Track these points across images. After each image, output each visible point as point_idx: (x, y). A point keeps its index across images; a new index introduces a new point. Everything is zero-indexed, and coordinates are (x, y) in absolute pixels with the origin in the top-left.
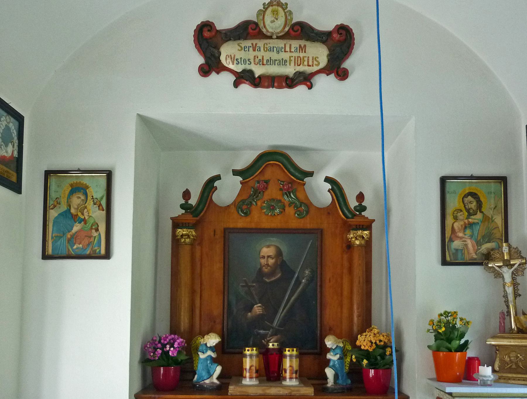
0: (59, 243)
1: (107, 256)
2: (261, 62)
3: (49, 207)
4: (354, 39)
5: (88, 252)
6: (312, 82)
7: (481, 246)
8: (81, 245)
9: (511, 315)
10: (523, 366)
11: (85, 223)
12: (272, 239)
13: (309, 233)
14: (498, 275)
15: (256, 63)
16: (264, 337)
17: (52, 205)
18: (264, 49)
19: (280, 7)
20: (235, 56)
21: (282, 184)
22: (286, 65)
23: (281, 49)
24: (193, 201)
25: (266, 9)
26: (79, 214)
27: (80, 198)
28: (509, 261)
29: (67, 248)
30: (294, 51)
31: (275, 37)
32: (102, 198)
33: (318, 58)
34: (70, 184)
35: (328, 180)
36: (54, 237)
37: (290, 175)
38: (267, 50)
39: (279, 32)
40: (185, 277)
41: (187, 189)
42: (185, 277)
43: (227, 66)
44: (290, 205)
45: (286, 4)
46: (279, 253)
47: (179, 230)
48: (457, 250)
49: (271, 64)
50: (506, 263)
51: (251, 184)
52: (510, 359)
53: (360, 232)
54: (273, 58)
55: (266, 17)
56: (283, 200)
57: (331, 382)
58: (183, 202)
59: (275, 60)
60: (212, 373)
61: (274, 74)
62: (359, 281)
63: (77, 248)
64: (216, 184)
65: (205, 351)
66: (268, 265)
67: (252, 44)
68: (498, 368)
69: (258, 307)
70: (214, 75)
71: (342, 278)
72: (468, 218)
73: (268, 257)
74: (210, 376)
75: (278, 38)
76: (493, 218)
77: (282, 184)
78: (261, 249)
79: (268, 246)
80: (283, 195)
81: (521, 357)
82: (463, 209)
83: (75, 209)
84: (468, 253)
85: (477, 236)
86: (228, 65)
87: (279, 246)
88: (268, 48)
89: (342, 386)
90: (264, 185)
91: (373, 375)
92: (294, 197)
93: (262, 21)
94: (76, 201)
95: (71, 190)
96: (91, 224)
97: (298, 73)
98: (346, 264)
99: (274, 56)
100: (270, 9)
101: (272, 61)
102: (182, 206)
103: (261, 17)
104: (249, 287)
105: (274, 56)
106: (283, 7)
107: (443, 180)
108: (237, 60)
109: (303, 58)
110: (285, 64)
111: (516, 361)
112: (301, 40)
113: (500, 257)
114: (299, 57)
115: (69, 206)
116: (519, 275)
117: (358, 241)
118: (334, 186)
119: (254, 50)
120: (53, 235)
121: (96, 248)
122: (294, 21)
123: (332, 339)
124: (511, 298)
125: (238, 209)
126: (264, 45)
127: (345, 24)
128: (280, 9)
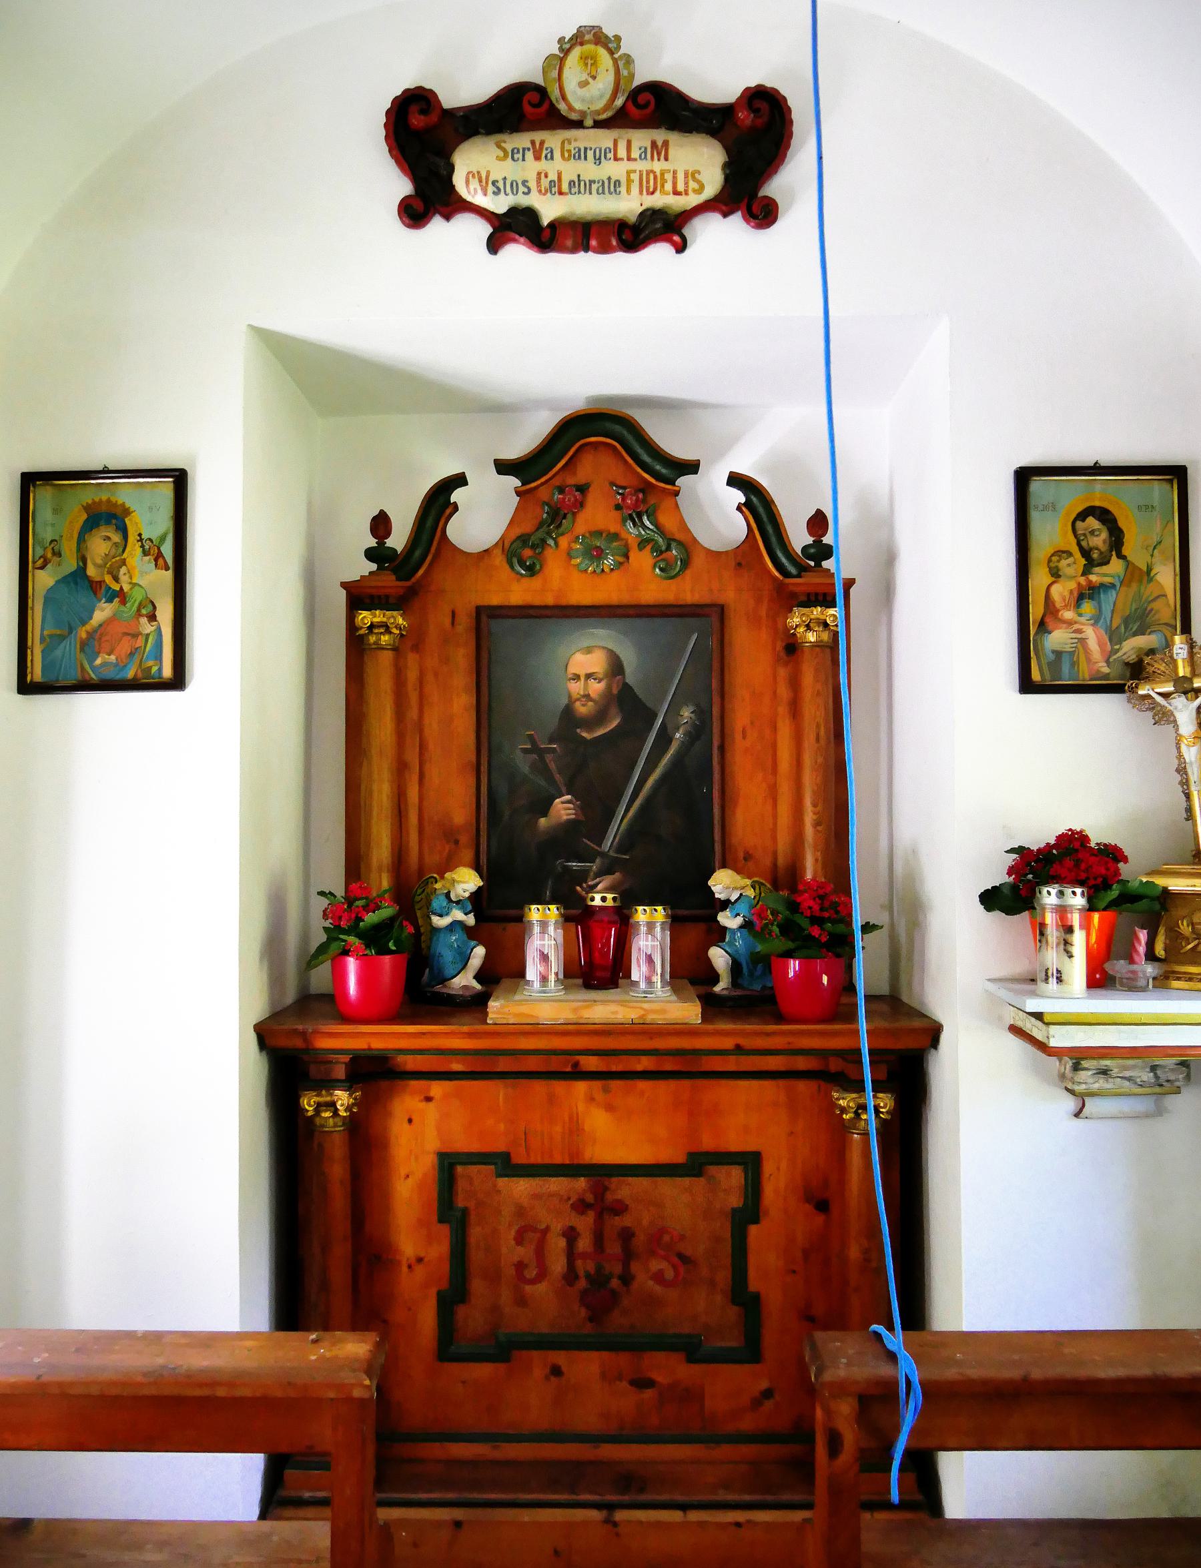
0: (58, 653)
1: (177, 682)
2: (555, 186)
3: (34, 562)
4: (791, 122)
5: (130, 674)
6: (685, 234)
7: (1121, 644)
8: (113, 658)
11: (123, 602)
14: (1164, 717)
15: (543, 191)
16: (582, 876)
17: (40, 558)
18: (562, 155)
19: (602, 47)
20: (488, 173)
22: (618, 193)
23: (605, 153)
24: (398, 540)
25: (567, 52)
26: (108, 579)
27: (108, 538)
28: (1189, 680)
29: (79, 666)
30: (638, 157)
31: (589, 122)
32: (163, 539)
33: (699, 172)
34: (85, 505)
35: (735, 480)
36: (47, 638)
37: (639, 470)
38: (570, 156)
39: (601, 109)
40: (382, 729)
42: (382, 729)
43: (469, 198)
44: (643, 543)
45: (618, 39)
46: (616, 667)
47: (364, 613)
48: (1058, 654)
49: (579, 192)
50: (1184, 686)
51: (544, 493)
52: (1193, 928)
53: (817, 612)
54: (586, 177)
55: (566, 73)
56: (624, 535)
58: (372, 542)
59: (590, 181)
61: (589, 218)
62: (818, 735)
63: (104, 664)
64: (457, 496)
66: (587, 696)
67: (533, 143)
68: (1163, 953)
69: (563, 803)
70: (437, 223)
71: (774, 728)
72: (1086, 572)
73: (589, 676)
75: (598, 124)
76: (1151, 570)
77: (620, 494)
79: (589, 650)
80: (624, 521)
82: (1075, 550)
83: (95, 565)
84: (1089, 660)
85: (1112, 617)
86: (473, 197)
88: (573, 152)
90: (575, 497)
91: (797, 969)
92: (652, 525)
93: (558, 84)
94: (100, 546)
95: (86, 521)
96: (136, 604)
97: (649, 213)
98: (784, 692)
99: (589, 170)
100: (577, 52)
101: (582, 183)
102: (370, 554)
103: (555, 74)
104: (541, 752)
105: (589, 170)
106: (610, 45)
107: (1024, 477)
108: (494, 183)
109: (662, 174)
110: (615, 191)
112: (657, 128)
113: (1167, 672)
114: (652, 171)
115: (83, 559)
117: (813, 634)
118: (752, 497)
119: (537, 158)
120: (46, 633)
121: (150, 663)
122: (638, 81)
124: (1196, 772)
125: (511, 558)
126: (563, 143)
127: (769, 84)
128: (602, 52)
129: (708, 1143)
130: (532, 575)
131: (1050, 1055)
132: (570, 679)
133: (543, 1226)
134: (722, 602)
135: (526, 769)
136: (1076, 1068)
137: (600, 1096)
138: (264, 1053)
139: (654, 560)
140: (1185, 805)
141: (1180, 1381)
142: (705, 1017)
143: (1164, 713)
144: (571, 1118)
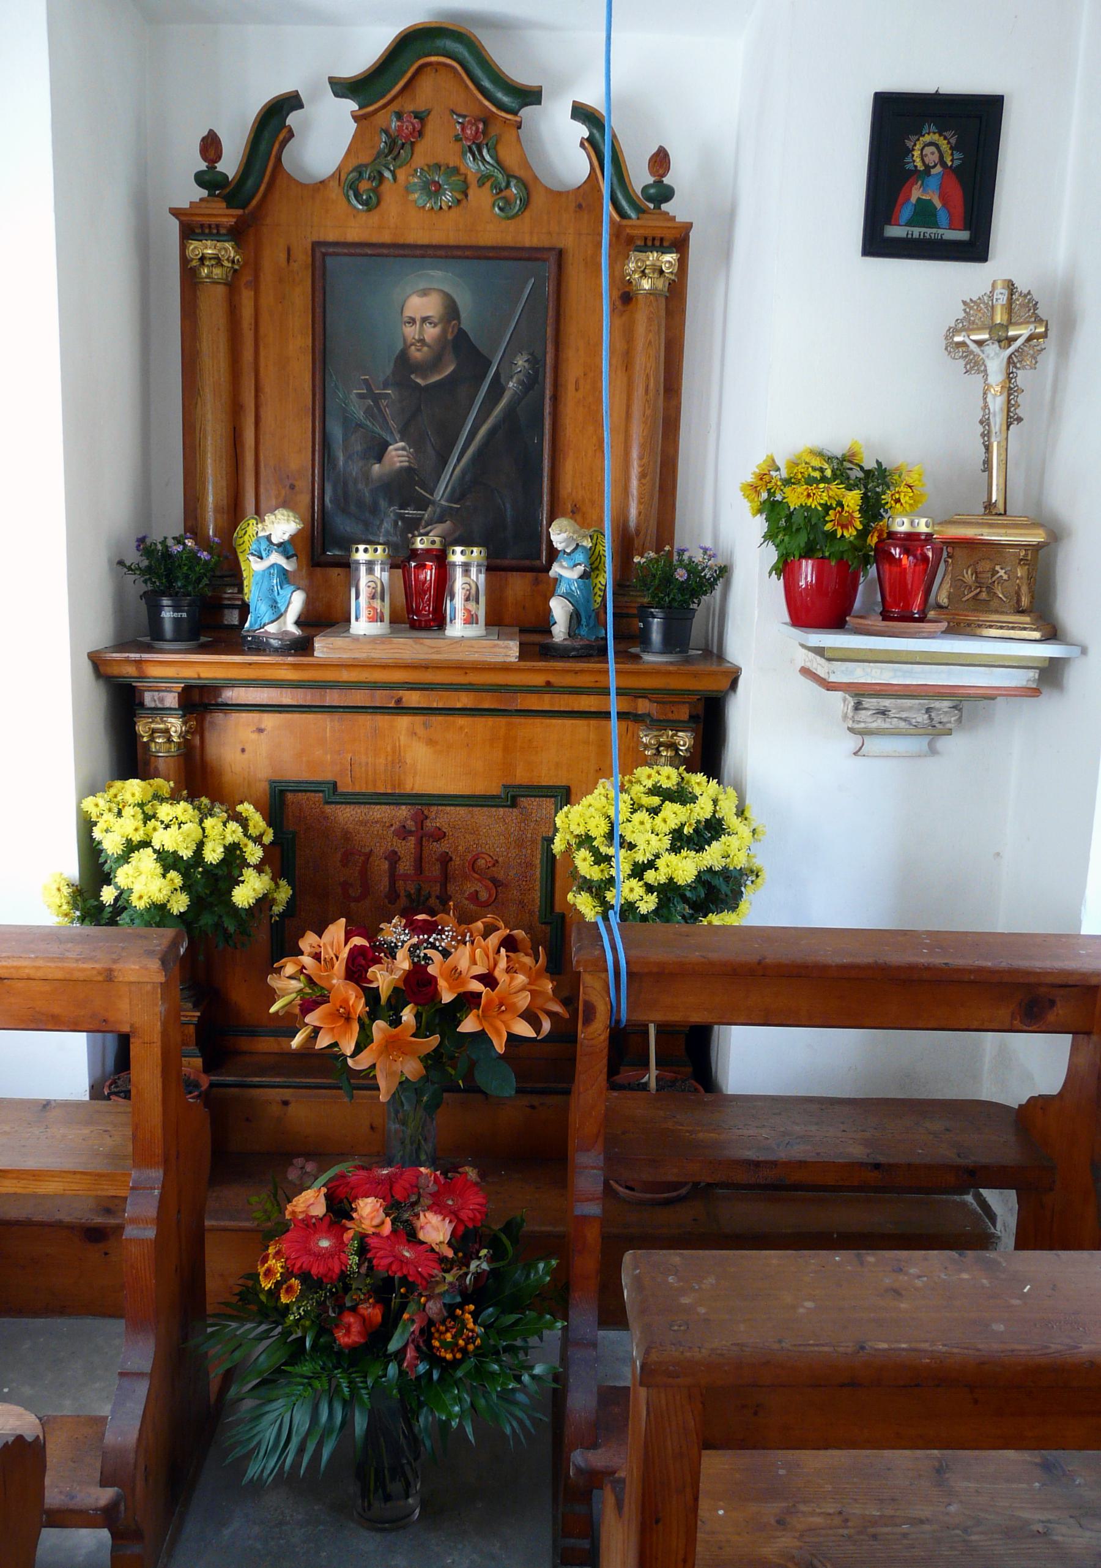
9: (992, 468)
10: (1003, 593)
12: (432, 272)
13: (529, 259)
21: (459, 123)
24: (229, 165)
35: (581, 113)
37: (480, 97)
41: (211, 131)
44: (483, 180)
46: (451, 311)
47: (195, 243)
52: (977, 577)
53: (653, 256)
56: (463, 170)
57: (559, 631)
58: (203, 166)
60: (283, 610)
65: (264, 555)
66: (422, 341)
68: (946, 600)
69: (396, 450)
73: (424, 320)
74: (279, 616)
78: (405, 301)
79: (424, 293)
81: (1002, 573)
87: (455, 296)
89: (587, 642)
90: (413, 124)
102: (201, 179)
104: (376, 398)
111: (990, 581)
116: (1024, 368)
123: (568, 528)
125: (348, 191)
129: (521, 776)
130: (369, 210)
131: (828, 690)
132: (405, 323)
133: (367, 850)
134: (561, 246)
135: (360, 414)
136: (858, 707)
137: (421, 731)
138: (101, 682)
139: (493, 200)
140: (983, 457)
141: (899, 968)
142: (522, 657)
143: (975, 363)
144: (394, 752)
